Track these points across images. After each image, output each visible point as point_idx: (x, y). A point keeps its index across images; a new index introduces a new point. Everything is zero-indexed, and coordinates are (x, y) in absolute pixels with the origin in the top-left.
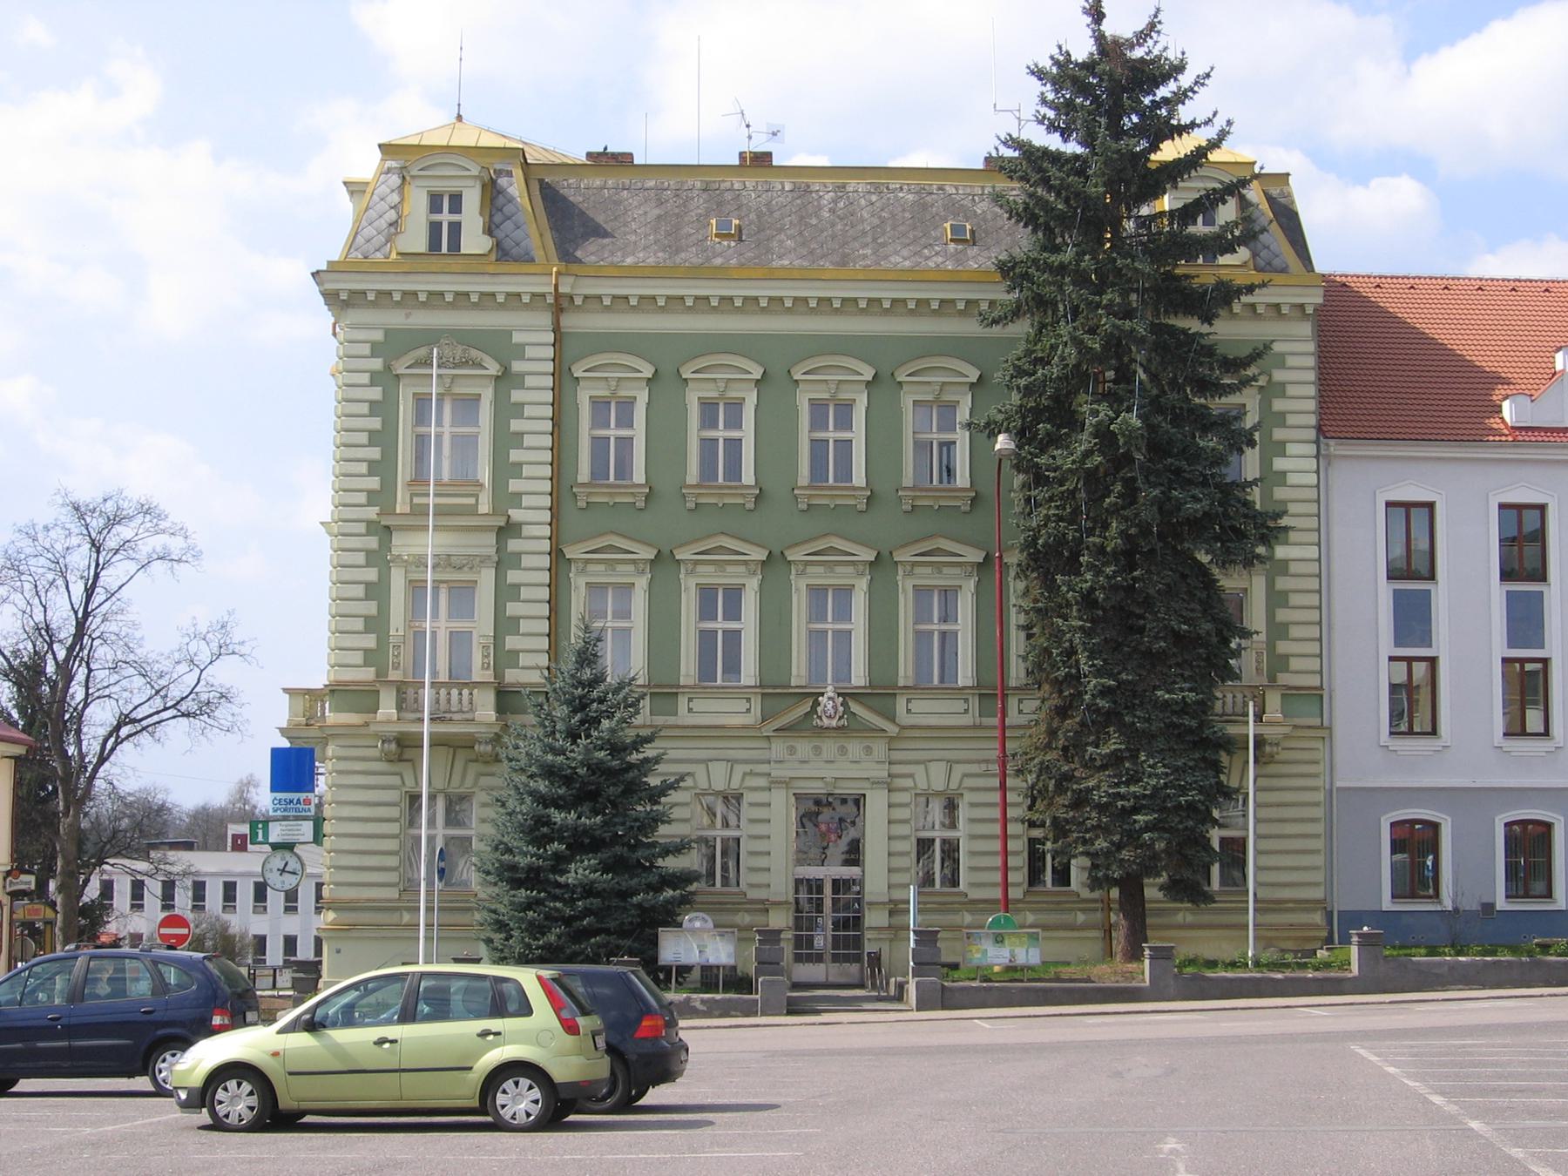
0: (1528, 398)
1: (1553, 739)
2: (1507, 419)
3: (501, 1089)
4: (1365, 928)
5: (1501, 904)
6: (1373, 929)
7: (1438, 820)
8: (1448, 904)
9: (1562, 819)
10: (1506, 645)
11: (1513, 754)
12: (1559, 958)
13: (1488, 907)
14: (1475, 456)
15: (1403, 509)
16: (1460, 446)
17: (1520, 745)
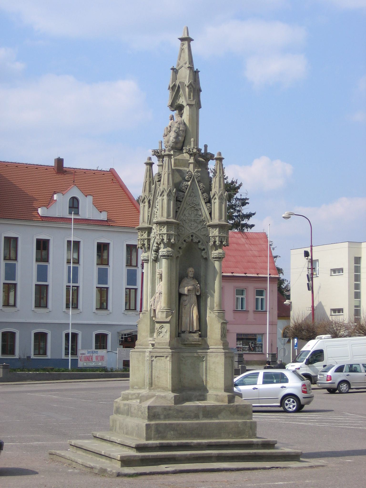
0: (46, 208)
1: (16, 307)
2: (40, 214)
3: (295, 401)
4: (4, 364)
5: (33, 357)
6: (6, 364)
7: (48, 333)
8: (17, 356)
9: (19, 331)
10: (4, 279)
11: (37, 313)
12: (100, 373)
13: (29, 357)
14: (14, 223)
15: (8, 240)
16: (27, 221)
17: (130, 313)
